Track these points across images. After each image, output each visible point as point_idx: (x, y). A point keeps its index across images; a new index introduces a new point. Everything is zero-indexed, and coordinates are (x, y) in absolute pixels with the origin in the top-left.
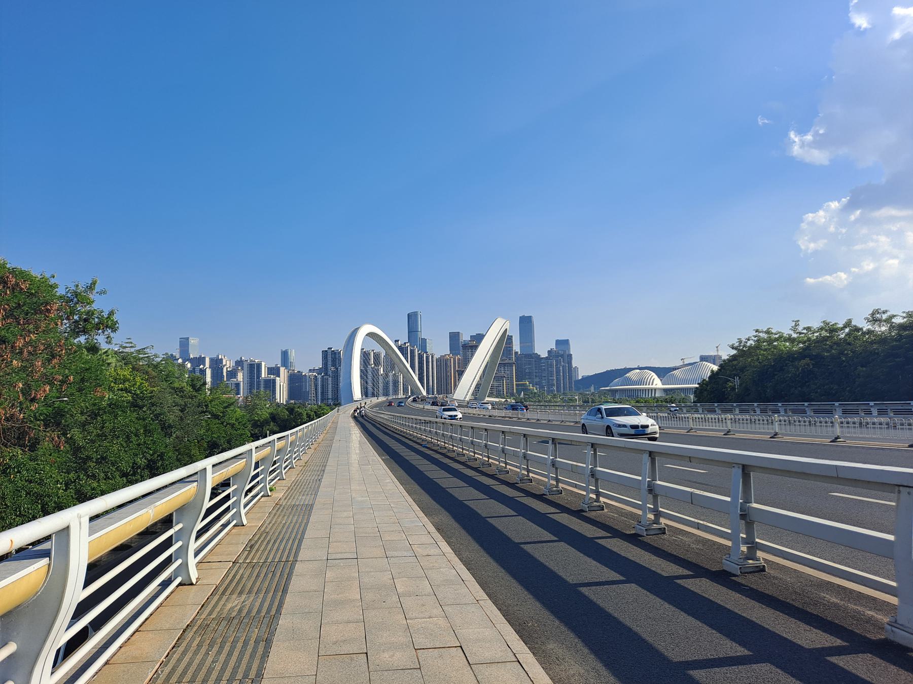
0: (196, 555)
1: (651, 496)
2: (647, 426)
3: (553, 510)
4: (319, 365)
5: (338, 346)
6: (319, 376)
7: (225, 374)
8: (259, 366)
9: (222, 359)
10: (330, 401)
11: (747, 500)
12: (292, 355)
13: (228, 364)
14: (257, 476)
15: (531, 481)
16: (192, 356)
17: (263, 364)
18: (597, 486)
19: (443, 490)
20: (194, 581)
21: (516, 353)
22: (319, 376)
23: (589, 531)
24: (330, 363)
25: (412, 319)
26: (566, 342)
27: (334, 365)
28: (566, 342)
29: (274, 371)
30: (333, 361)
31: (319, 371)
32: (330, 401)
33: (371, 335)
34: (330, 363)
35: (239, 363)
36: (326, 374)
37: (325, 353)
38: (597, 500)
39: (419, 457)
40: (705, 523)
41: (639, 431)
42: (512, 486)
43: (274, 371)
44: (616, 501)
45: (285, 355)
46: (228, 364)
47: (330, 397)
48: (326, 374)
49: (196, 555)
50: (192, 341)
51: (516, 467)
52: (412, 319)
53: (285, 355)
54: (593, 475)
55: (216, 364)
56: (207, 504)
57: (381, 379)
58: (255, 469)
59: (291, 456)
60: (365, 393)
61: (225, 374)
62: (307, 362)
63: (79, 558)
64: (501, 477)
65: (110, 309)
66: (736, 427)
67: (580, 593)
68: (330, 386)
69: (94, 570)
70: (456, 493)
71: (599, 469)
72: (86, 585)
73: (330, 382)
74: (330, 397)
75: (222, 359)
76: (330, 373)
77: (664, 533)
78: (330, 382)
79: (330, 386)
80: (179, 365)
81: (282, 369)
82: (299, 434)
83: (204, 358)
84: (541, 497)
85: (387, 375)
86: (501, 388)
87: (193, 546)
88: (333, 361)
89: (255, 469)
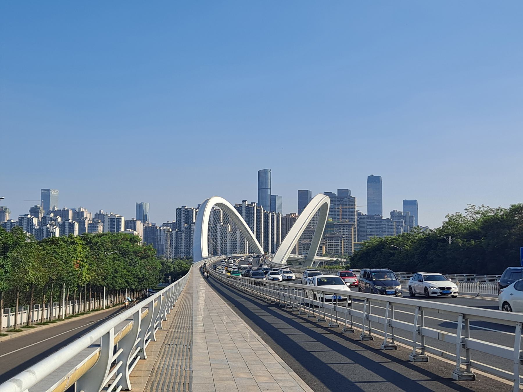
1: (464, 350)
2: (450, 288)
3: (385, 359)
4: (173, 219)
5: (191, 205)
6: (174, 232)
7: (86, 226)
8: (119, 220)
9: (83, 212)
10: (183, 255)
12: (147, 207)
13: (88, 216)
15: (395, 348)
16: (56, 209)
17: (123, 219)
18: (468, 357)
19: (285, 336)
21: (359, 214)
22: (174, 232)
24: (183, 220)
25: (263, 177)
27: (187, 222)
29: (131, 225)
30: (185, 218)
31: (173, 226)
32: (183, 255)
33: (218, 204)
34: (183, 220)
35: (99, 216)
36: (180, 230)
37: (179, 211)
38: (468, 370)
39: (288, 326)
41: (445, 293)
42: (378, 351)
43: (131, 225)
44: (405, 344)
45: (140, 207)
46: (88, 216)
47: (183, 251)
48: (180, 230)
50: (53, 193)
51: (381, 334)
52: (263, 177)
53: (140, 207)
54: (464, 346)
55: (79, 216)
57: (229, 236)
60: (213, 252)
61: (86, 226)
62: (162, 216)
65: (79, 207)
67: (298, 345)
68: (183, 241)
70: (294, 339)
71: (470, 339)
73: (183, 238)
74: (183, 251)
75: (83, 212)
76: (183, 229)
77: (396, 349)
78: (183, 238)
79: (183, 241)
81: (138, 223)
83: (68, 211)
84: (406, 363)
85: (234, 232)
86: (339, 248)
88: (185, 218)
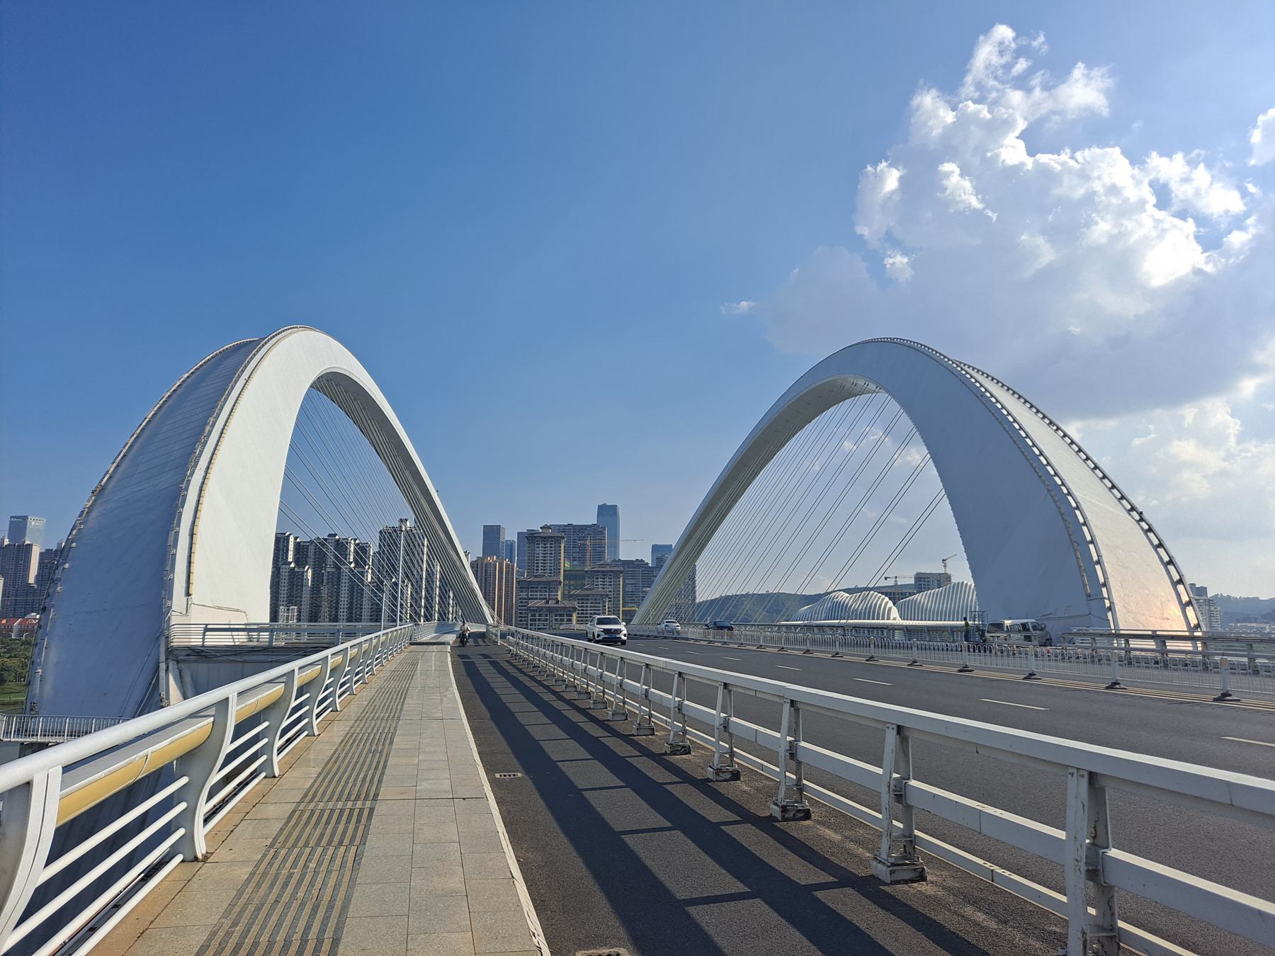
0: (206, 821)
11: (1098, 844)
14: (299, 707)
20: (200, 856)
23: (714, 813)
26: (613, 509)
28: (613, 509)
40: (1007, 873)
46: (510, 535)
49: (206, 821)
50: (33, 523)
56: (228, 747)
58: (299, 695)
59: (351, 679)
63: (43, 821)
64: (641, 739)
66: (845, 650)
69: (66, 837)
70: (536, 733)
72: (50, 860)
80: (1204, 644)
82: (365, 646)
87: (203, 808)
89: (299, 695)
